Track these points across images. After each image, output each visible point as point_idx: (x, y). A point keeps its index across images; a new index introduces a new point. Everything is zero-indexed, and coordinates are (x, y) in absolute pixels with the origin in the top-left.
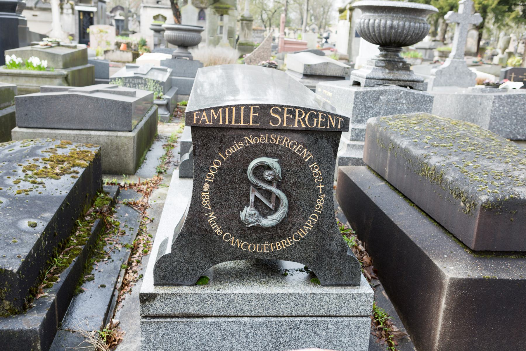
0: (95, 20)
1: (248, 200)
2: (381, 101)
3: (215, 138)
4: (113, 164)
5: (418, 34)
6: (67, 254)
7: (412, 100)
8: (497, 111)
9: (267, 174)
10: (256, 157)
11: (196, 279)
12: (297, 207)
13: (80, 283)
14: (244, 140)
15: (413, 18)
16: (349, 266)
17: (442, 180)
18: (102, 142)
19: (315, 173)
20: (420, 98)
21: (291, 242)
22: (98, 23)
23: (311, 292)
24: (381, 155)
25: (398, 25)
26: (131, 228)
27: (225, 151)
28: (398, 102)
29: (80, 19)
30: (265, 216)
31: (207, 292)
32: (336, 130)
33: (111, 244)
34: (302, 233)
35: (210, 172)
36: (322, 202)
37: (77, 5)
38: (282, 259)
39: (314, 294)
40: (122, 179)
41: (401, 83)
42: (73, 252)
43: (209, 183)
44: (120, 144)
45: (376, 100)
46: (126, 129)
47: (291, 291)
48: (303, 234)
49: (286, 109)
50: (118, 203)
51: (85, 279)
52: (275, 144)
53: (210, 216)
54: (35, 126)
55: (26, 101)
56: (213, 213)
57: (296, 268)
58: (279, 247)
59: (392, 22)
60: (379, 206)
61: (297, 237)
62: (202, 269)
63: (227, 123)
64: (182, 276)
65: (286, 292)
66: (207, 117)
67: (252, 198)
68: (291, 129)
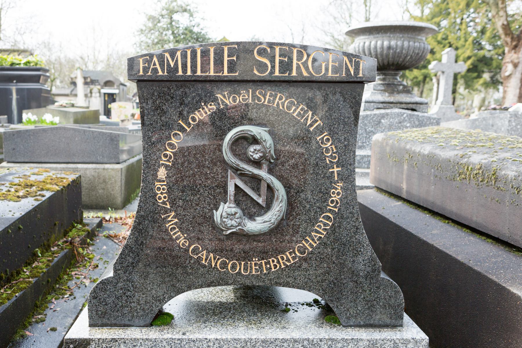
0: (117, 99)
1: (226, 192)
2: (383, 124)
3: (172, 98)
4: (100, 198)
5: (418, 54)
6: (10, 289)
7: (417, 123)
8: (514, 131)
9: (252, 150)
10: (235, 125)
11: (151, 316)
12: (301, 203)
13: (25, 325)
14: (215, 100)
15: (412, 38)
16: (385, 296)
17: (496, 179)
18: (89, 175)
19: (327, 148)
20: (425, 120)
21: (294, 258)
22: (120, 101)
23: (327, 337)
24: (394, 171)
25: (397, 45)
26: (106, 261)
27: (188, 116)
28: (402, 126)
29: (105, 100)
30: (251, 217)
31: (166, 336)
32: (355, 80)
33: (78, 278)
34: (310, 244)
35: (166, 150)
36: (338, 194)
37: (102, 88)
38: (280, 284)
39: (332, 340)
40: (108, 213)
41: (403, 106)
42: (18, 286)
43: (166, 167)
44: (107, 177)
45: (377, 124)
46: (113, 161)
47: (296, 335)
48: (311, 245)
49: (277, 49)
50: (98, 235)
51: (34, 320)
52: (263, 105)
53: (170, 219)
54: (23, 160)
55: (14, 135)
56: (173, 214)
57: (302, 302)
58: (275, 266)
59: (390, 42)
60: (401, 225)
61: (302, 250)
62: (159, 301)
63: (189, 73)
64: (130, 312)
65: (289, 337)
66: (160, 65)
67: (231, 189)
68: (287, 79)
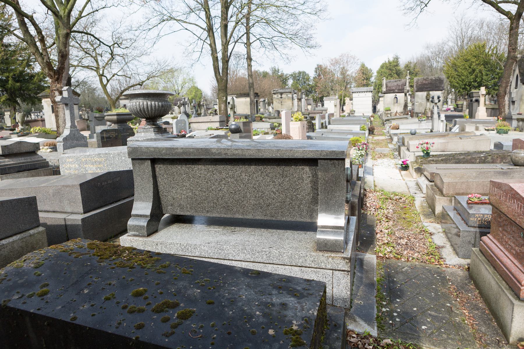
46: (35, 225)
